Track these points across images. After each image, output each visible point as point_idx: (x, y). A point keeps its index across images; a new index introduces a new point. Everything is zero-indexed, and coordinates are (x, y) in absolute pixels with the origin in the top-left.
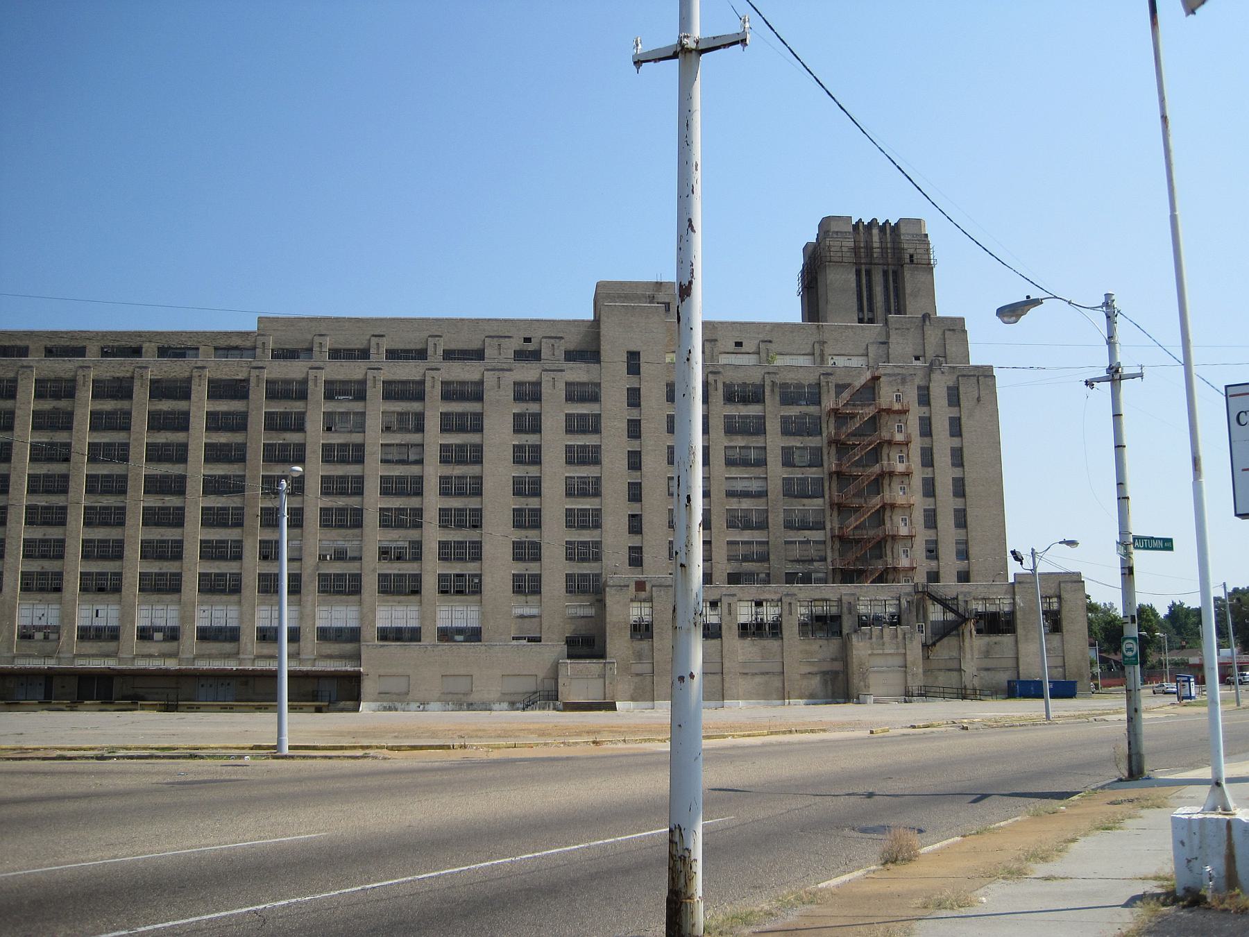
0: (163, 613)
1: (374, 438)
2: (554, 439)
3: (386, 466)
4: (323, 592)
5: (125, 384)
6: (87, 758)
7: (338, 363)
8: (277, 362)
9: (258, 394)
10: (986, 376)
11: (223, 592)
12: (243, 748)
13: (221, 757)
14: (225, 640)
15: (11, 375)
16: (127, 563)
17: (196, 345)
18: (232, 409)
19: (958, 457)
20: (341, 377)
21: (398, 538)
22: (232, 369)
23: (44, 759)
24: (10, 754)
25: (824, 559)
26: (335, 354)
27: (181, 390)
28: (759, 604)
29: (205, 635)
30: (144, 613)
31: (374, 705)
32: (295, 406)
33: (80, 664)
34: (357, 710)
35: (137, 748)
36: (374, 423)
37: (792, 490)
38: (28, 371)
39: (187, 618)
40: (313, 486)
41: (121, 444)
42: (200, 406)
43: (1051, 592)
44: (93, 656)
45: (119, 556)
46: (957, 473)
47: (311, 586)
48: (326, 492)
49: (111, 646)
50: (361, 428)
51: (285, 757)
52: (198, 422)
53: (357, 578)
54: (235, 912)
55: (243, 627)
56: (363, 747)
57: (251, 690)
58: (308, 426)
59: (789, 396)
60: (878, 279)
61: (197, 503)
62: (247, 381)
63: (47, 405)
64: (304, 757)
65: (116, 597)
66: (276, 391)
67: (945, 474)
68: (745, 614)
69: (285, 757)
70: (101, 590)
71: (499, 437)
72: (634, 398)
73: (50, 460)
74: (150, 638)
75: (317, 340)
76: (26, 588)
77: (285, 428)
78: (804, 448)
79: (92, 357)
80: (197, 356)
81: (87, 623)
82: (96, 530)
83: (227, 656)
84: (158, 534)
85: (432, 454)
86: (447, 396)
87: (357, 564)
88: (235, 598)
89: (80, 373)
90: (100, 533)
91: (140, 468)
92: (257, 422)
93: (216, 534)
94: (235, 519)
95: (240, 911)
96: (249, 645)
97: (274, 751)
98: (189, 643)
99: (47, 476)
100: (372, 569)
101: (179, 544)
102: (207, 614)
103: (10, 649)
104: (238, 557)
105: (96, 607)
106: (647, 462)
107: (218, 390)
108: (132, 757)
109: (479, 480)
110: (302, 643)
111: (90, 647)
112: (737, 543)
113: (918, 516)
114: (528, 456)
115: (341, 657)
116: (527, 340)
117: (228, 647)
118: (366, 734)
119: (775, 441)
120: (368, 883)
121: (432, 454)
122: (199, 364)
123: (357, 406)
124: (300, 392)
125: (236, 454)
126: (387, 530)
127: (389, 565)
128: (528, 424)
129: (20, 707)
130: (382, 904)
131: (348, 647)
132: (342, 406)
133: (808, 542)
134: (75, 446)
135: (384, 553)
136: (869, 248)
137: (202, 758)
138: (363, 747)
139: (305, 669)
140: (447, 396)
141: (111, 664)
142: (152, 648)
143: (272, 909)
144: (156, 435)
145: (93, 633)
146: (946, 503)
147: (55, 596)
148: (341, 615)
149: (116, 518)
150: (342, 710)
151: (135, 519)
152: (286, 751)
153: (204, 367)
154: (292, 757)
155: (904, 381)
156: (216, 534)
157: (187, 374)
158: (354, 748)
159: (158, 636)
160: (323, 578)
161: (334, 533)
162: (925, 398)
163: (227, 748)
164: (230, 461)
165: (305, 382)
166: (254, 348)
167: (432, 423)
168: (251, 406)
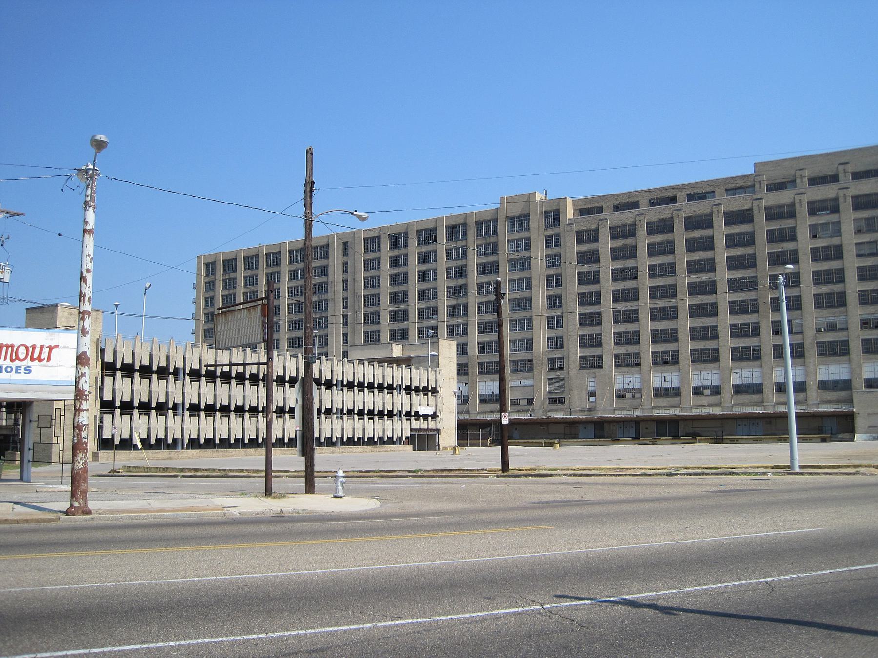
0: (707, 376)
3: (860, 259)
4: (821, 355)
5: (667, 223)
6: (661, 475)
7: (815, 188)
8: (771, 194)
9: (760, 218)
11: (748, 359)
12: (767, 468)
13: (751, 474)
14: (753, 393)
15: (594, 226)
16: (681, 343)
17: (712, 189)
18: (743, 230)
20: (819, 198)
21: (829, 315)
22: (739, 202)
23: (634, 475)
24: (613, 472)
26: (813, 181)
27: (706, 222)
29: (739, 389)
30: (695, 377)
31: (865, 436)
32: (788, 223)
33: (656, 413)
34: (853, 440)
35: (693, 468)
36: (848, 228)
38: (605, 222)
39: (725, 378)
40: (807, 278)
41: (670, 264)
42: (721, 231)
44: (665, 407)
45: (676, 340)
47: (811, 352)
48: (817, 282)
49: (676, 400)
50: (838, 233)
51: (797, 474)
52: (720, 243)
53: (846, 344)
54: (752, 581)
55: (765, 383)
56: (855, 467)
57: (771, 427)
58: (799, 236)
61: (725, 299)
62: (751, 209)
63: (619, 243)
64: (811, 474)
65: (676, 366)
66: (773, 214)
69: (797, 474)
70: (666, 363)
73: (625, 279)
74: (702, 394)
75: (799, 173)
76: (618, 365)
77: (782, 240)
79: (644, 207)
80: (714, 197)
81: (659, 386)
82: (659, 323)
83: (755, 404)
84: (700, 322)
86: (770, 217)
87: (845, 333)
88: (758, 363)
89: (638, 219)
90: (662, 325)
91: (684, 279)
92: (761, 238)
93: (740, 319)
94: (753, 308)
95: (755, 581)
96: (770, 396)
97: (789, 470)
98: (728, 396)
99: (624, 290)
100: (856, 336)
101: (715, 328)
102: (739, 375)
103: (612, 405)
104: (757, 334)
105: (666, 375)
107: (732, 218)
108: (690, 474)
110: (808, 393)
111: (662, 401)
115: (838, 401)
117: (756, 397)
118: (858, 457)
120: (853, 566)
122: (716, 202)
123: (834, 218)
124: (790, 212)
125: (749, 262)
126: (865, 307)
127: (870, 332)
128: (589, 258)
129: (620, 442)
130: (863, 582)
131: (843, 394)
132: (823, 218)
134: (640, 268)
135: (865, 324)
137: (738, 474)
138: (855, 467)
139: (812, 411)
140: (770, 217)
141: (677, 412)
142: (704, 400)
143: (779, 581)
144: (693, 254)
145: (663, 392)
147: (637, 368)
148: (835, 371)
149: (671, 314)
150: (841, 440)
151: (684, 313)
152: (797, 470)
153: (720, 204)
154: (802, 474)
156: (740, 319)
157: (709, 211)
158: (848, 467)
159: (707, 392)
160: (820, 345)
161: (826, 312)
163: (755, 468)
164: (745, 267)
165: (793, 205)
166: (753, 186)
168: (756, 227)
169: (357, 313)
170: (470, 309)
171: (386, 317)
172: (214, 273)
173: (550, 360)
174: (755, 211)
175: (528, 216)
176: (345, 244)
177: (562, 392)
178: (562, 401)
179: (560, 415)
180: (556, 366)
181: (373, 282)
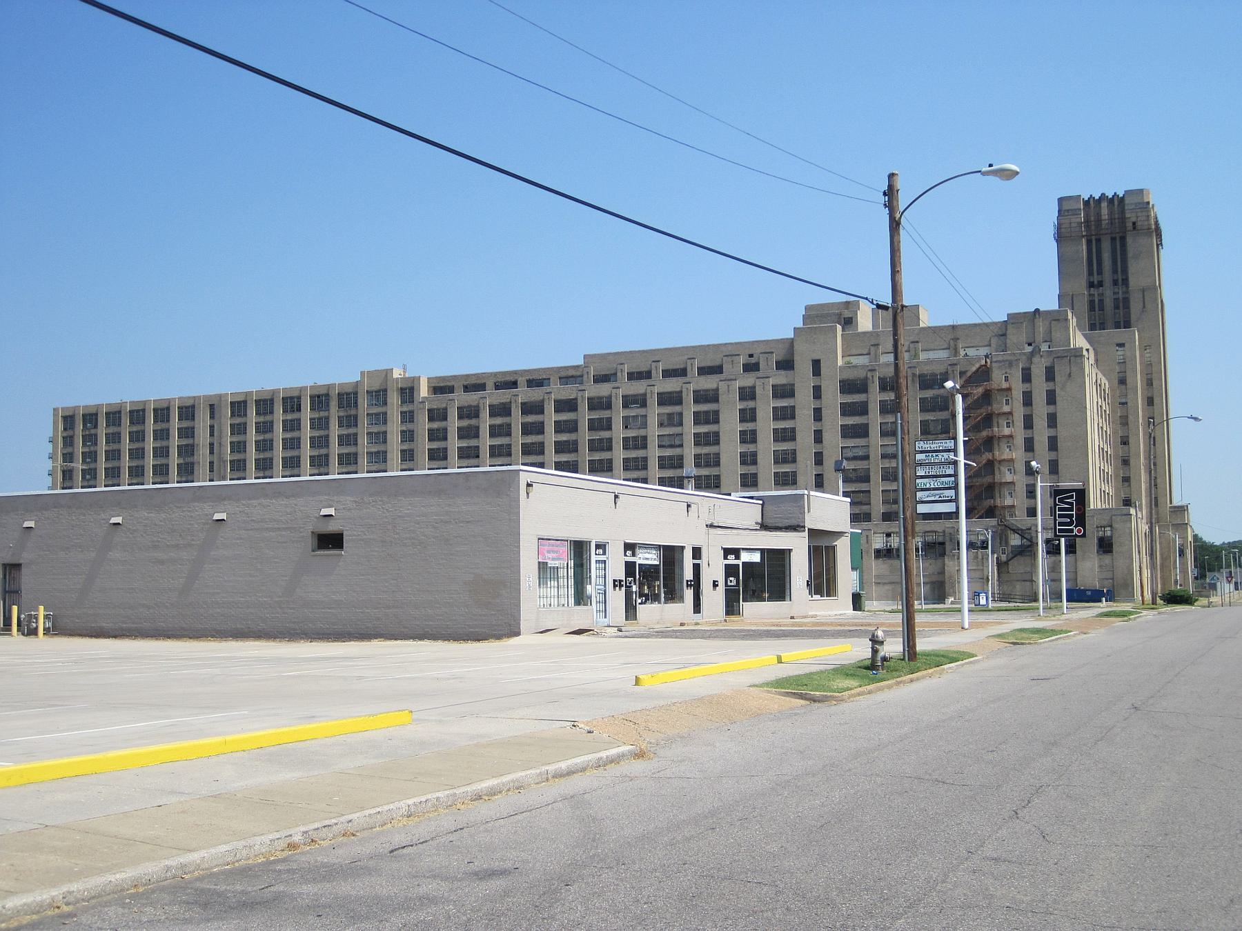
1: (653, 431)
2: (766, 425)
9: (584, 406)
19: (1052, 420)
22: (567, 392)
28: (888, 535)
36: (653, 421)
43: (1105, 523)
46: (1052, 432)
50: (644, 425)
52: (550, 428)
60: (1106, 245)
68: (878, 542)
71: (730, 425)
72: (817, 392)
85: (689, 440)
109: (717, 455)
114: (749, 437)
116: (751, 356)
121: (689, 440)
123: (641, 411)
128: (748, 416)
136: (1099, 220)
155: (1011, 364)
162: (1027, 378)
167: (689, 419)
175: (385, 390)
176: (212, 406)
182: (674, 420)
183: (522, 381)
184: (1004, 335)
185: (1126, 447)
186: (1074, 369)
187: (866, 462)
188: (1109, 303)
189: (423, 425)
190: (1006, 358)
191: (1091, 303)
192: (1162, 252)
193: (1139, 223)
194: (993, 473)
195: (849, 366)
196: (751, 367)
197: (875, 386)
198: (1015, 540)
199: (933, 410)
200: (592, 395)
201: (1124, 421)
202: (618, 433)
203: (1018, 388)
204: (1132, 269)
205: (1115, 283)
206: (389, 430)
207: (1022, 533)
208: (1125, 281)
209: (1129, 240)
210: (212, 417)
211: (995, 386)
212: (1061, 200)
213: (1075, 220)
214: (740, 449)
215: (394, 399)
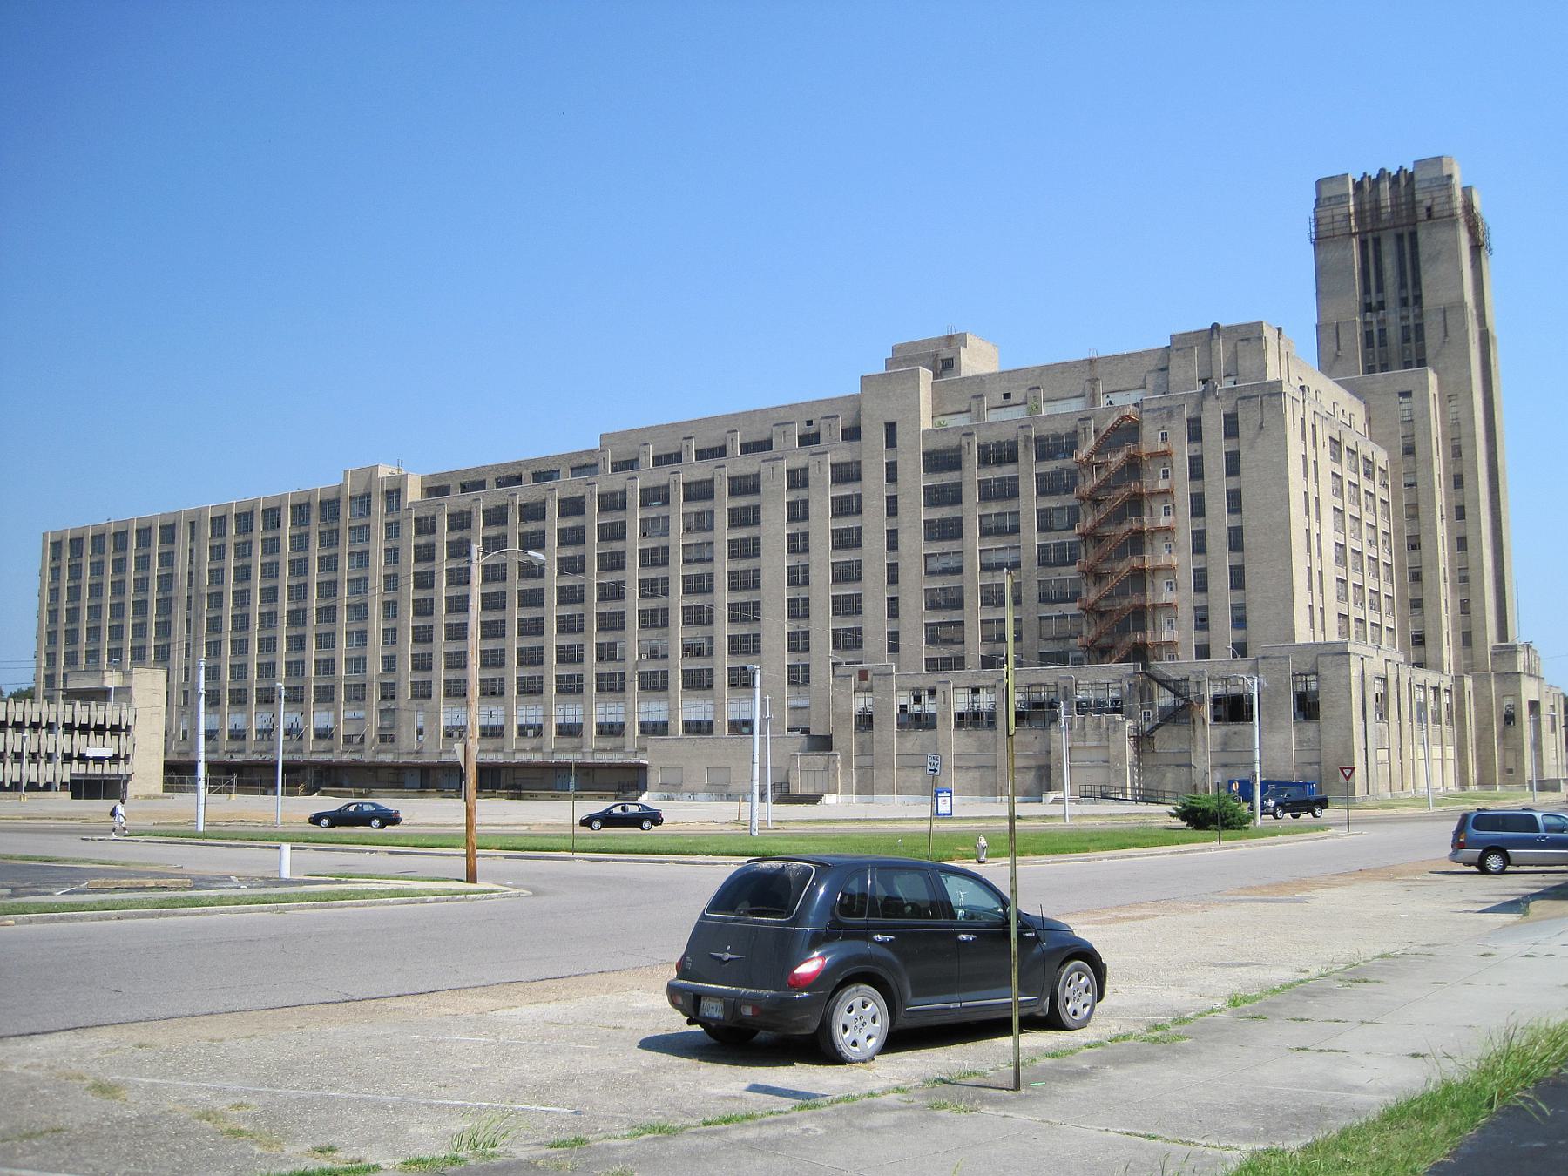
1: (677, 538)
2: (822, 524)
10: (1271, 395)
19: (1235, 501)
21: (697, 633)
25: (1080, 634)
28: (975, 691)
37: (1047, 557)
43: (1306, 668)
46: (1235, 521)
49: (617, 741)
59: (1047, 448)
67: (1218, 524)
68: (961, 702)
71: (775, 527)
75: (643, 449)
78: (1062, 508)
79: (491, 489)
106: (903, 540)
112: (991, 622)
113: (1186, 579)
114: (799, 544)
116: (810, 423)
119: (1029, 503)
123: (662, 511)
128: (799, 512)
133: (1064, 617)
136: (1377, 208)
146: (1220, 558)
155: (1170, 415)
162: (1195, 434)
169: (201, 617)
170: (671, 586)
171: (475, 603)
172: (222, 534)
173: (383, 685)
174: (587, 500)
175: (369, 496)
176: (192, 523)
177: (392, 728)
178: (392, 739)
179: (388, 758)
180: (388, 692)
181: (217, 576)
182: (702, 523)
183: (527, 474)
184: (1166, 369)
185: (1415, 553)
186: (1267, 417)
187: (958, 577)
188: (1394, 333)
189: (410, 539)
190: (1164, 403)
191: (1368, 336)
192: (1489, 265)
193: (1436, 209)
194: (1144, 590)
195: (942, 430)
196: (809, 440)
197: (972, 458)
198: (1165, 699)
199: (1055, 492)
200: (605, 489)
201: (1413, 511)
202: (634, 543)
203: (1182, 451)
204: (1425, 280)
205: (1404, 302)
206: (371, 548)
207: (1175, 687)
208: (1418, 299)
209: (1422, 236)
210: (192, 539)
211: (1145, 449)
212: (1319, 183)
213: (1339, 211)
214: (787, 562)
215: (379, 506)
